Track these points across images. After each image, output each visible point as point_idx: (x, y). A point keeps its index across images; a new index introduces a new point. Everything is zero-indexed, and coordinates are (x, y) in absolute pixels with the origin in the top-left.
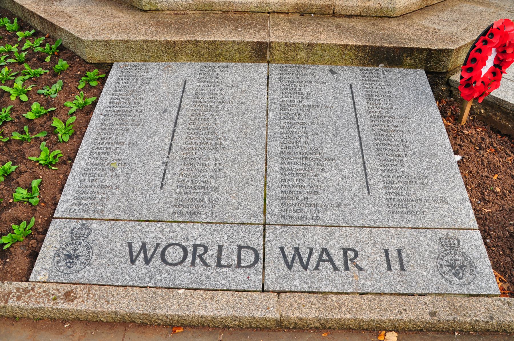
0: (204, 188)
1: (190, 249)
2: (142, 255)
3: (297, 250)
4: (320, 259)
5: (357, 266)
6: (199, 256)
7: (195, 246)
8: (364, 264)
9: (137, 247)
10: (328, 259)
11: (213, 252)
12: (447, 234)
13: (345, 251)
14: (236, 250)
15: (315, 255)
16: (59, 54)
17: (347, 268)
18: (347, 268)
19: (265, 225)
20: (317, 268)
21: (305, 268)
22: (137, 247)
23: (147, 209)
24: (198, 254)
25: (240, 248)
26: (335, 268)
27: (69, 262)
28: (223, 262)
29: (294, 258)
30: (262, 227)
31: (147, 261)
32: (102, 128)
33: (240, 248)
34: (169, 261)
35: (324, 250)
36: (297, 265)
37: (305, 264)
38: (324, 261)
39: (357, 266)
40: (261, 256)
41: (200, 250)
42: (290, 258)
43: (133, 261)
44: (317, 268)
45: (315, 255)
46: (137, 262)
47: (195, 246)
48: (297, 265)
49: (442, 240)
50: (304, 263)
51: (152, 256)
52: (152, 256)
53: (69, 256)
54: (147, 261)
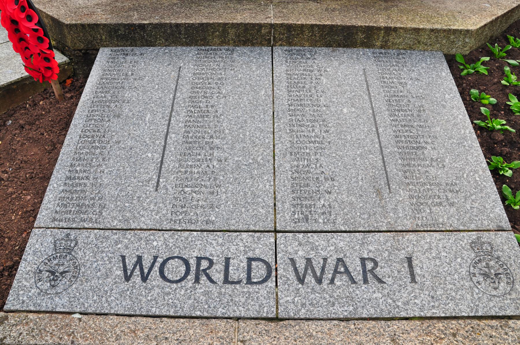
0: (17, 330)
1: (193, 262)
2: (137, 272)
3: (309, 261)
4: (336, 271)
7: (199, 259)
9: (130, 262)
11: (219, 267)
12: (478, 238)
13: (363, 260)
14: (244, 264)
17: (366, 281)
18: (366, 281)
19: (276, 231)
20: (332, 281)
21: (319, 281)
22: (130, 262)
23: (252, 91)
24: (202, 268)
25: (250, 260)
29: (306, 269)
30: (279, 235)
31: (144, 278)
32: (101, 86)
33: (250, 260)
34: (170, 277)
36: (309, 279)
37: (301, 277)
38: (340, 273)
40: (156, 268)
41: (204, 264)
42: (301, 271)
43: (127, 278)
46: (132, 280)
47: (199, 259)
48: (309, 279)
50: (139, 266)
51: (134, 268)
52: (134, 268)
54: (144, 278)
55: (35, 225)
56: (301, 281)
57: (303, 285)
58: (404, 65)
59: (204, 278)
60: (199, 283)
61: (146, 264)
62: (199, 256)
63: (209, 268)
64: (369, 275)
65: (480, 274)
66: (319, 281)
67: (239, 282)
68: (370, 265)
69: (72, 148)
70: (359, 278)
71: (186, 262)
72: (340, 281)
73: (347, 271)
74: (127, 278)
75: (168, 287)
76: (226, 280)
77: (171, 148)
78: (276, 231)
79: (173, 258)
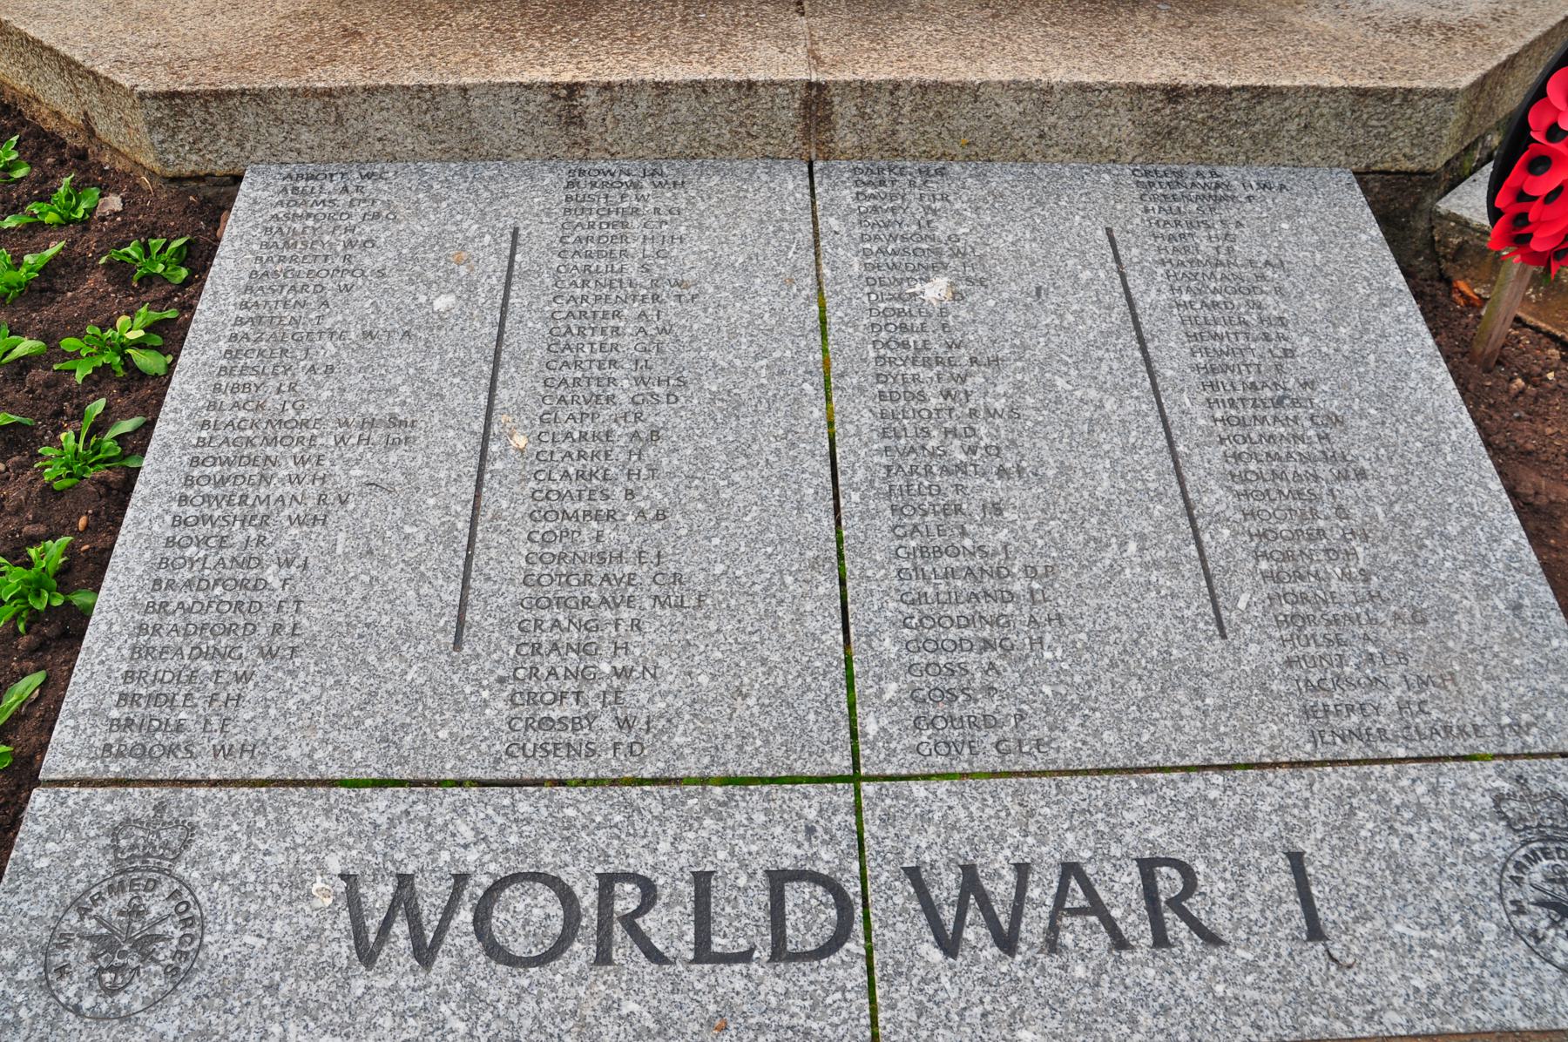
2: (400, 928)
5: (1195, 925)
6: (1168, 902)
8: (1219, 921)
9: (946, 887)
10: (1086, 903)
13: (1148, 867)
15: (1041, 892)
16: (1553, 392)
17: (1161, 940)
18: (1161, 940)
20: (1052, 945)
25: (778, 880)
26: (1120, 943)
27: (110, 969)
28: (718, 944)
31: (424, 954)
35: (1070, 870)
39: (1195, 925)
40: (465, 916)
41: (627, 899)
43: (367, 955)
44: (1052, 945)
45: (1041, 892)
47: (607, 883)
49: (827, 837)
53: (105, 944)
54: (424, 954)
55: (53, 764)
56: (950, 945)
57: (368, 969)
58: (1219, 195)
59: (623, 948)
60: (609, 961)
61: (1001, 889)
62: (1147, 855)
63: (643, 909)
64: (618, 931)
65: (1540, 903)
66: (1007, 942)
67: (746, 957)
68: (1168, 882)
69: (179, 459)
70: (1136, 927)
71: (567, 897)
72: (1077, 933)
73: (1096, 906)
74: (367, 955)
75: (498, 985)
76: (703, 952)
77: (854, 474)
78: (855, 778)
79: (535, 877)
